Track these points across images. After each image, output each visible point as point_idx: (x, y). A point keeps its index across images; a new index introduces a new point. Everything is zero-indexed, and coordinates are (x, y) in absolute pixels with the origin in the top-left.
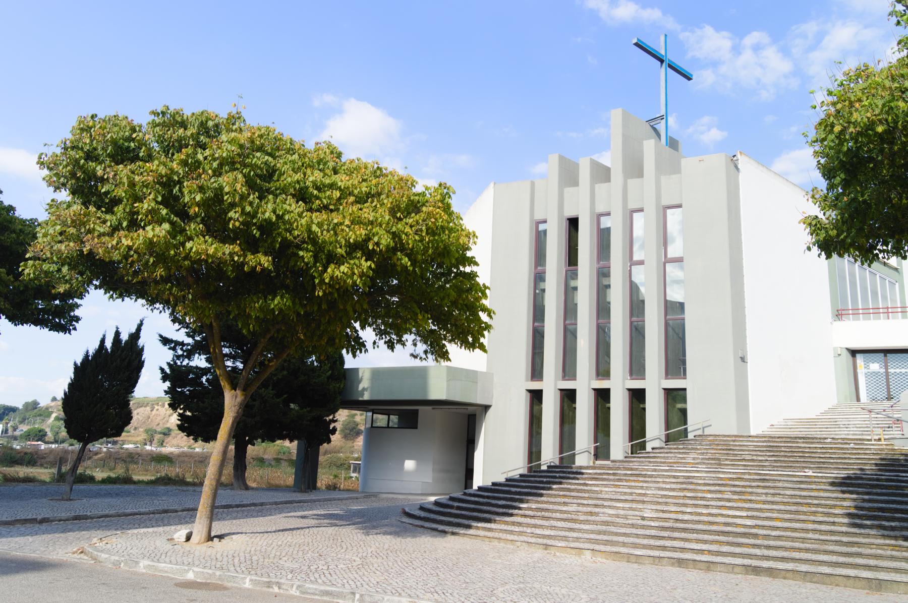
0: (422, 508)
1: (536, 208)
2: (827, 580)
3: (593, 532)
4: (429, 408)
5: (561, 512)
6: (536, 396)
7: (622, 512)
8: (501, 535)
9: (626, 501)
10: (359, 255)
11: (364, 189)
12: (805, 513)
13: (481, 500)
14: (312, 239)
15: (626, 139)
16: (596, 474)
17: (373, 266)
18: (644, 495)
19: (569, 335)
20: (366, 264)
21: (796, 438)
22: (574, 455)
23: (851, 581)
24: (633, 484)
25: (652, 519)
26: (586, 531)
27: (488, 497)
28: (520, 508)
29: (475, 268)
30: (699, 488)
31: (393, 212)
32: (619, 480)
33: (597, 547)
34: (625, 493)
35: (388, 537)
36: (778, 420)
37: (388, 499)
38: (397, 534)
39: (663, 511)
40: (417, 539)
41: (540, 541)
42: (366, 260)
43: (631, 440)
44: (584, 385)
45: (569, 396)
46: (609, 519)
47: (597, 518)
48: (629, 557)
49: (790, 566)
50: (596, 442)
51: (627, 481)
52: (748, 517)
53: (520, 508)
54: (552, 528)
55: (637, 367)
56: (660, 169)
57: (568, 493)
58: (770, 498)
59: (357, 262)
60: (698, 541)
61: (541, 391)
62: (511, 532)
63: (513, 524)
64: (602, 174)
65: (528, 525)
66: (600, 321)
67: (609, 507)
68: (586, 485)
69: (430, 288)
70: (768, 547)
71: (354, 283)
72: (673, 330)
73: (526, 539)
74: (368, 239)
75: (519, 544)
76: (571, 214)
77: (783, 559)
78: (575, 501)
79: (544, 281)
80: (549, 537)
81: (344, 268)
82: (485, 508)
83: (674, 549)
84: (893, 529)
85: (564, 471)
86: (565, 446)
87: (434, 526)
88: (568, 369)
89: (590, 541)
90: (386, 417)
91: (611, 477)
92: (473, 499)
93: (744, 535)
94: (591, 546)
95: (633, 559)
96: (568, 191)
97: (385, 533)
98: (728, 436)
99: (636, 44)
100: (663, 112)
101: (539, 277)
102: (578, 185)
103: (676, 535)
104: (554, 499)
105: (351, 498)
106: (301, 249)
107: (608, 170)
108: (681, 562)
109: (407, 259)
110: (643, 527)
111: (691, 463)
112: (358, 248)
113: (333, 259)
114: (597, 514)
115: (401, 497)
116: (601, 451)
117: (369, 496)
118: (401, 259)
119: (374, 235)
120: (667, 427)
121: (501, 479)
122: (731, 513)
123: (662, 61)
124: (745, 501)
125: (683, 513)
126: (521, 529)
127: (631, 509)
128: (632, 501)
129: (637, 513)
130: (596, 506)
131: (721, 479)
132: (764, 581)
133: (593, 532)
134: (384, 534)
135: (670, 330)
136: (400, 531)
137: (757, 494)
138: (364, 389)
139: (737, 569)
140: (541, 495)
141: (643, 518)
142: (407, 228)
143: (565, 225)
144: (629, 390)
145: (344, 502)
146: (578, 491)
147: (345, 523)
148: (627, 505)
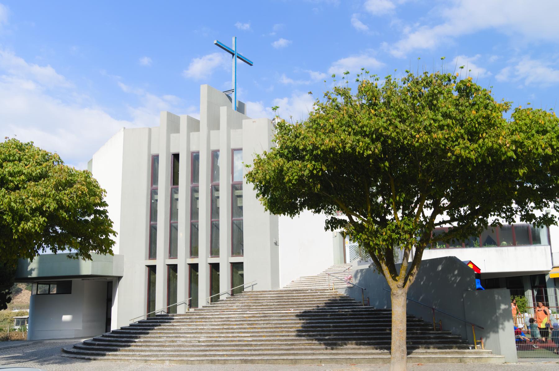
0: (75, 347)
1: (152, 146)
2: (275, 362)
3: (172, 351)
4: (80, 279)
5: (157, 342)
6: (152, 269)
7: (188, 339)
8: (123, 358)
9: (192, 333)
10: (38, 214)
11: (39, 171)
12: (278, 332)
13: (112, 339)
14: (11, 209)
15: (210, 105)
16: (180, 319)
17: (46, 220)
18: (203, 329)
19: (173, 229)
20: (42, 220)
21: (293, 291)
22: (176, 305)
23: (285, 361)
24: (198, 323)
25: (203, 342)
26: (168, 351)
27: (117, 337)
28: (135, 342)
29: (106, 208)
30: (232, 323)
31: (56, 187)
32: (192, 322)
33: (172, 358)
34: (193, 329)
35: (55, 365)
36: (296, 278)
37: (50, 344)
38: (60, 363)
39: (210, 337)
40: (73, 364)
41: (143, 358)
42: (42, 217)
43: (211, 294)
44: (183, 261)
45: (173, 269)
46: (181, 343)
47: (175, 344)
48: (187, 362)
49: (260, 358)
50: (190, 297)
51: (196, 322)
52: (251, 336)
53: (135, 342)
54: (151, 351)
55: (214, 251)
56: (230, 125)
57: (162, 331)
58: (265, 326)
59: (37, 218)
60: (223, 350)
61: (155, 266)
62: (128, 355)
63: (130, 351)
64: (194, 125)
65: (138, 351)
66: (193, 221)
67: (183, 337)
68: (173, 325)
69: (80, 221)
70: (255, 350)
71: (36, 231)
72: (236, 225)
73: (135, 358)
74: (43, 204)
75: (131, 361)
76: (175, 151)
77: (259, 355)
78: (166, 335)
79: (157, 194)
80: (148, 356)
81: (30, 224)
82: (114, 343)
83: (211, 355)
84: (313, 335)
85: (164, 319)
86: (171, 300)
87: (83, 356)
88: (172, 252)
89: (169, 356)
90: (48, 286)
91: (188, 320)
92: (107, 339)
93: (246, 345)
94: (169, 358)
95: (189, 362)
96: (173, 136)
97: (53, 363)
98: (259, 292)
99: (216, 44)
100: (233, 88)
101: (154, 192)
102: (179, 133)
103: (214, 348)
104: (157, 336)
105: (23, 346)
106: (4, 215)
107: (198, 122)
108: (212, 362)
109: (65, 214)
110: (198, 346)
111: (232, 309)
112: (39, 210)
113: (22, 218)
114: (176, 341)
115: (60, 341)
116: (193, 303)
117: (36, 342)
118: (62, 214)
119: (46, 203)
120: (233, 286)
121: (127, 324)
122: (243, 335)
123: (233, 55)
124: (252, 328)
125: (220, 337)
126: (133, 353)
127: (194, 337)
128: (196, 333)
129: (197, 339)
130: (176, 337)
131: (245, 317)
132: (249, 366)
133: (172, 351)
134: (52, 364)
135: (235, 226)
136: (63, 361)
137: (259, 324)
138: (32, 269)
139: (238, 362)
140: (148, 333)
141: (199, 342)
142: (65, 197)
143: (171, 158)
144: (210, 264)
145: (19, 348)
146: (168, 329)
147: (25, 360)
148: (192, 335)
